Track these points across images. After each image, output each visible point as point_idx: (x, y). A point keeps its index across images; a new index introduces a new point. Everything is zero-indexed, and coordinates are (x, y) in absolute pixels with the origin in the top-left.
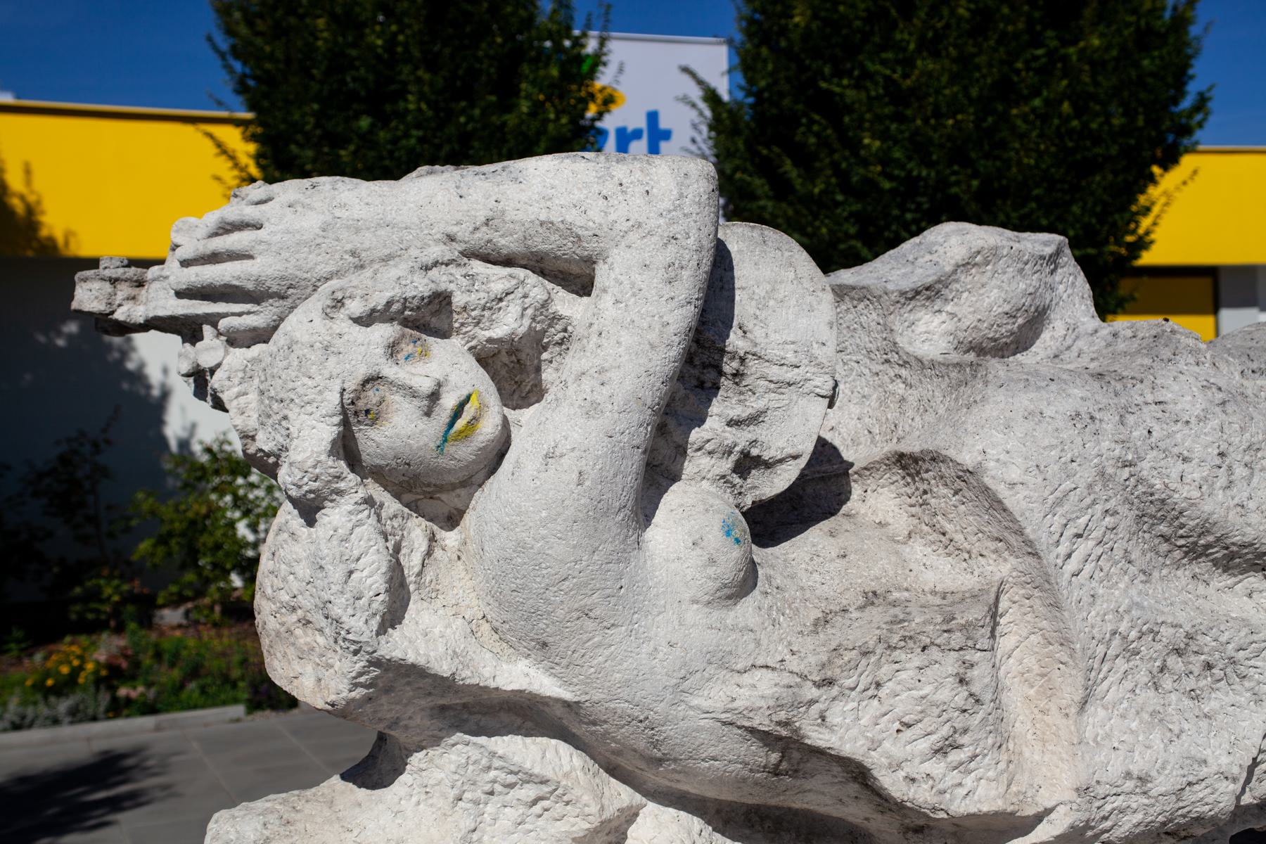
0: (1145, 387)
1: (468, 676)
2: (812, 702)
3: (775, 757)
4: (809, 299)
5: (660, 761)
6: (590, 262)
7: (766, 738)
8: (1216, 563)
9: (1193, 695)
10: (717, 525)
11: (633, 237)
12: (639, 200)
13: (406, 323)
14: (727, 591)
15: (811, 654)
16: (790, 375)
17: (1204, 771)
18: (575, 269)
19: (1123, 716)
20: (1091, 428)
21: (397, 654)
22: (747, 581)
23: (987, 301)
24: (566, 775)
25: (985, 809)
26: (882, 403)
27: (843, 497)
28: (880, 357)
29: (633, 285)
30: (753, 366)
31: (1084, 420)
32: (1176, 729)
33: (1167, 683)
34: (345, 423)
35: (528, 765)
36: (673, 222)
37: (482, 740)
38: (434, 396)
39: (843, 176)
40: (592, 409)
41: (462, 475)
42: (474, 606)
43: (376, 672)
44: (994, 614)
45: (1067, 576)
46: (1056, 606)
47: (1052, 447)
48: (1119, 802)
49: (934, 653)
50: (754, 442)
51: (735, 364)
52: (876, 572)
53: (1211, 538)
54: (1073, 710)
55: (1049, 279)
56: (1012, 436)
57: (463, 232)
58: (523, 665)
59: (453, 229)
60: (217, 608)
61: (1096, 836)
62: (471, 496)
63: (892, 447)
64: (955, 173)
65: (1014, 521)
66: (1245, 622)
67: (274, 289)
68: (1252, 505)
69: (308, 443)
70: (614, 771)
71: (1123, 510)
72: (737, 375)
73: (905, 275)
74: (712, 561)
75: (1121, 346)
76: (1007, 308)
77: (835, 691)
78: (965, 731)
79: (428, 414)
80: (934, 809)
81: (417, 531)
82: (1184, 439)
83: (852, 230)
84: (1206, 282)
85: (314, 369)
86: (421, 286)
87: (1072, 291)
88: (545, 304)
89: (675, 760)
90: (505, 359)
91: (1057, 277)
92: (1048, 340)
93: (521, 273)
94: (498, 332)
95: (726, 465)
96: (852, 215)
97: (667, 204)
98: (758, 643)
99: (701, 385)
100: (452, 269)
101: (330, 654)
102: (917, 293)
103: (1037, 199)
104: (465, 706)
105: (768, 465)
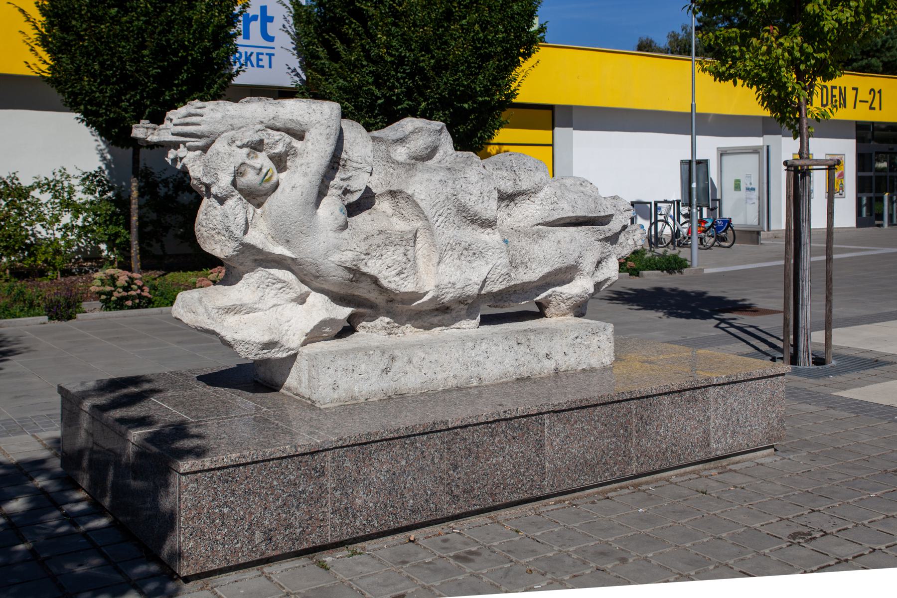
0: (462, 173)
1: (266, 249)
3: (351, 276)
6: (304, 132)
7: (349, 269)
9: (470, 262)
11: (317, 125)
12: (319, 115)
13: (252, 148)
15: (363, 247)
16: (359, 166)
22: (345, 226)
23: (419, 144)
27: (373, 204)
30: (349, 162)
33: (463, 258)
38: (261, 169)
39: (367, 53)
40: (305, 174)
42: (266, 230)
46: (432, 235)
49: (398, 247)
56: (422, 186)
57: (266, 121)
58: (280, 248)
60: (8, 271)
63: (387, 189)
64: (423, 56)
69: (225, 180)
70: (303, 281)
75: (458, 160)
81: (251, 208)
82: (471, 188)
83: (370, 81)
84: (550, 112)
86: (256, 138)
87: (447, 141)
88: (290, 143)
92: (438, 156)
93: (283, 134)
94: (277, 151)
95: (340, 192)
96: (370, 72)
99: (333, 168)
103: (462, 71)
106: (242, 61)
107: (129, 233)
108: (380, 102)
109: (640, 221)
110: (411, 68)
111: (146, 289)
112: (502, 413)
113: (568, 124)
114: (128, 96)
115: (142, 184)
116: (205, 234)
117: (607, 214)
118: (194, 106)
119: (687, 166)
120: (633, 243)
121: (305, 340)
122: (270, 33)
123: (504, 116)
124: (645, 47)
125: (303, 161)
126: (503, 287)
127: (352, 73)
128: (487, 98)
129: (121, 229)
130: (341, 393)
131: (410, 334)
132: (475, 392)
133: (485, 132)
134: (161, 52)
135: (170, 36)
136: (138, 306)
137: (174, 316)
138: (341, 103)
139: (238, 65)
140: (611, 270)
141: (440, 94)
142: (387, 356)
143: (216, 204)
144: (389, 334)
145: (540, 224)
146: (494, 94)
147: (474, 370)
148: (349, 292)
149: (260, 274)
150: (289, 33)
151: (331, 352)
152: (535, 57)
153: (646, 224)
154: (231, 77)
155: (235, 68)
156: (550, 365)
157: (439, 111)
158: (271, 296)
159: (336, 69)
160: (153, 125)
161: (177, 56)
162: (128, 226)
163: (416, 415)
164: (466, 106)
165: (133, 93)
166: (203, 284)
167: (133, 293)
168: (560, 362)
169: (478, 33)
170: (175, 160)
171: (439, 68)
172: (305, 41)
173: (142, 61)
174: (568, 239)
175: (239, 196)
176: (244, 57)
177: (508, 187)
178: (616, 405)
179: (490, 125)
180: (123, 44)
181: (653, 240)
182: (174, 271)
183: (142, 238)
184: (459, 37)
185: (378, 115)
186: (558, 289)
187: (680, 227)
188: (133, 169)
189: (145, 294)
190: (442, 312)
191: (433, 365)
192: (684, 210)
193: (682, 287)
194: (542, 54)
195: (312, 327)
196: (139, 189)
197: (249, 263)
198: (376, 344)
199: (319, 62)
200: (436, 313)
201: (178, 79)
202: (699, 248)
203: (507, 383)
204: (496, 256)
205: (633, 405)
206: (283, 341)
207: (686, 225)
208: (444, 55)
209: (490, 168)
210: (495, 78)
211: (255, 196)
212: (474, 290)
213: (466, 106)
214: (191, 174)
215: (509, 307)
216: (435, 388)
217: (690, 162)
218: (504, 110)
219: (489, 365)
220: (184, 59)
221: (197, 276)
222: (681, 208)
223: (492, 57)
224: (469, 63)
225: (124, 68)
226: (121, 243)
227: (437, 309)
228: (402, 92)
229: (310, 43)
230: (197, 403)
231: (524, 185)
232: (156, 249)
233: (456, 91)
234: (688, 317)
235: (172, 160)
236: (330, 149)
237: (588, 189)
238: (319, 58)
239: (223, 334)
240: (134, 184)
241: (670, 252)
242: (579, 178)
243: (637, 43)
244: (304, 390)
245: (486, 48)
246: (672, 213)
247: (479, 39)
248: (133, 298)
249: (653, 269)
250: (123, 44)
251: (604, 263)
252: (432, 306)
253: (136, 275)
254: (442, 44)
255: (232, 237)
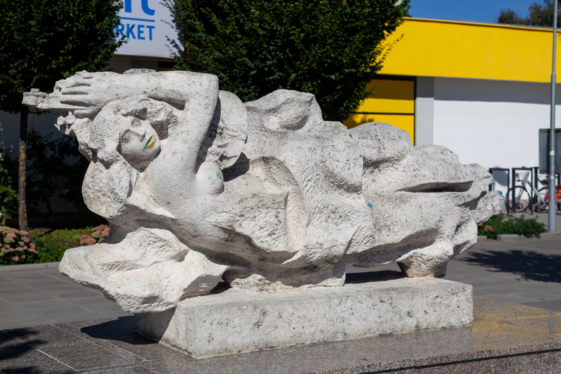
0: (330, 141)
2: (238, 221)
3: (227, 236)
4: (241, 113)
5: (196, 236)
6: (184, 102)
7: (225, 230)
8: (345, 190)
9: (336, 224)
10: (215, 173)
11: (197, 96)
13: (136, 116)
14: (217, 191)
15: (238, 209)
16: (235, 134)
17: (337, 243)
18: (179, 103)
19: (318, 229)
20: (314, 152)
21: (132, 203)
22: (221, 190)
23: (290, 114)
24: (171, 239)
25: (280, 250)
26: (259, 142)
27: (247, 169)
28: (259, 129)
29: (196, 109)
30: (225, 131)
31: (312, 150)
32: (331, 232)
33: (330, 220)
34: (120, 142)
35: (161, 236)
36: (207, 93)
37: (149, 229)
38: (144, 136)
39: (241, 27)
40: (185, 142)
41: (147, 158)
42: (149, 193)
43: (125, 208)
44: (286, 200)
45: (305, 191)
46: (302, 199)
47: (303, 157)
48: (315, 250)
49: (270, 209)
50: (225, 152)
51: (220, 130)
52: (256, 189)
53: (344, 183)
54: (305, 226)
55: (309, 108)
56: (294, 153)
57: (149, 91)
59: (146, 90)
61: (309, 260)
62: (149, 163)
64: (293, 30)
65: (292, 176)
66: (351, 205)
67: (94, 103)
68: (354, 174)
69: (109, 148)
70: (182, 240)
71: (321, 174)
72: (221, 133)
73: (267, 105)
74: (214, 183)
75: (326, 129)
76: (296, 116)
77: (244, 218)
78: (277, 230)
79: (141, 141)
80: (267, 250)
81: (134, 171)
82: (338, 156)
83: (244, 53)
84: (411, 83)
85: (112, 128)
86: (140, 107)
87: (316, 111)
88: (171, 112)
89: (200, 236)
90: (159, 126)
91: (311, 107)
92: (308, 125)
93: (165, 103)
94: (159, 119)
95: (217, 158)
97: (206, 88)
98: (224, 205)
99: (211, 136)
100: (146, 101)
101: (112, 203)
102: (271, 110)
104: (144, 220)
105: (228, 158)
106: (125, 32)
107: (17, 193)
108: (253, 73)
109: (498, 187)
110: (282, 41)
111: (33, 245)
112: (366, 367)
113: (429, 94)
114: (16, 64)
115: (30, 147)
116: (92, 196)
117: (466, 180)
118: (82, 76)
119: (545, 135)
120: (491, 208)
121: (183, 295)
122: (151, 6)
123: (369, 87)
124: (507, 19)
125: (183, 129)
126: (367, 248)
127: (227, 45)
128: (353, 70)
129: (9, 189)
130: (215, 346)
131: (280, 290)
132: (341, 346)
133: (350, 102)
134: (47, 23)
135: (56, 8)
136: (25, 262)
137: (61, 271)
138: (217, 74)
139: (120, 36)
140: (470, 234)
141: (309, 66)
142: (258, 311)
143: (102, 168)
144: (261, 290)
145: (402, 190)
146: (359, 67)
147: (340, 325)
148: (225, 250)
149: (142, 233)
150: (169, 7)
151: (207, 307)
152: (399, 30)
153: (504, 190)
154: (114, 47)
155: (118, 39)
156: (411, 323)
157: (308, 82)
158: (152, 253)
159: (212, 42)
160: (43, 94)
161: (63, 27)
162: (15, 186)
163: (285, 367)
164: (333, 77)
165: (21, 61)
166: (87, 241)
167: (20, 249)
168: (421, 320)
169: (345, 8)
170: (64, 127)
171: (308, 41)
172: (183, 14)
173: (29, 31)
174: (429, 204)
175: (124, 160)
176: (126, 29)
177: (373, 155)
178: (475, 364)
179: (356, 95)
180: (11, 14)
181: (511, 205)
182: (59, 228)
183: (29, 197)
184: (328, 12)
185: (251, 85)
186: (419, 251)
187: (538, 193)
188: (21, 133)
189: (32, 250)
190: (310, 271)
191: (301, 321)
192: (542, 177)
193: (539, 251)
194: (405, 28)
195: (189, 283)
196: (27, 152)
197: (132, 223)
198: (249, 299)
199: (196, 35)
200: (304, 271)
201: (64, 49)
202: (557, 214)
203: (370, 338)
204: (361, 219)
205: (492, 364)
206: (163, 296)
207: (544, 191)
208: (313, 29)
209: (356, 136)
210: (361, 51)
211: (138, 162)
212: (340, 250)
213: (333, 77)
214: (79, 139)
215: (372, 267)
216: (303, 342)
217: (549, 131)
218: (369, 81)
219: (353, 321)
220: (70, 30)
221: (81, 234)
222: (539, 175)
223: (359, 31)
224: (337, 37)
225: (12, 37)
226: (9, 202)
227: (305, 268)
228: (274, 64)
229: (188, 17)
230: (81, 353)
231: (388, 153)
232: (42, 208)
233: (324, 63)
234: (545, 280)
235: (61, 126)
236: (208, 118)
237: (448, 157)
238: (196, 31)
239: (107, 288)
240: (22, 147)
241: (528, 216)
242: (440, 147)
243: (498, 15)
244: (181, 342)
245: (353, 22)
246: (529, 179)
247: (346, 14)
248: (19, 254)
249: (510, 233)
250: (11, 14)
251: (463, 227)
252: (301, 265)
253: (22, 232)
254: (311, 18)
255: (117, 198)
